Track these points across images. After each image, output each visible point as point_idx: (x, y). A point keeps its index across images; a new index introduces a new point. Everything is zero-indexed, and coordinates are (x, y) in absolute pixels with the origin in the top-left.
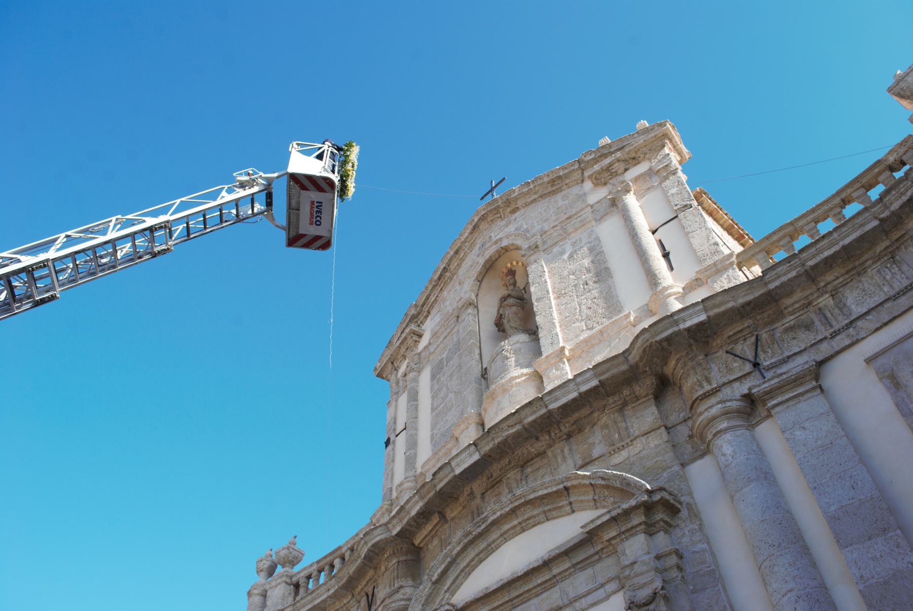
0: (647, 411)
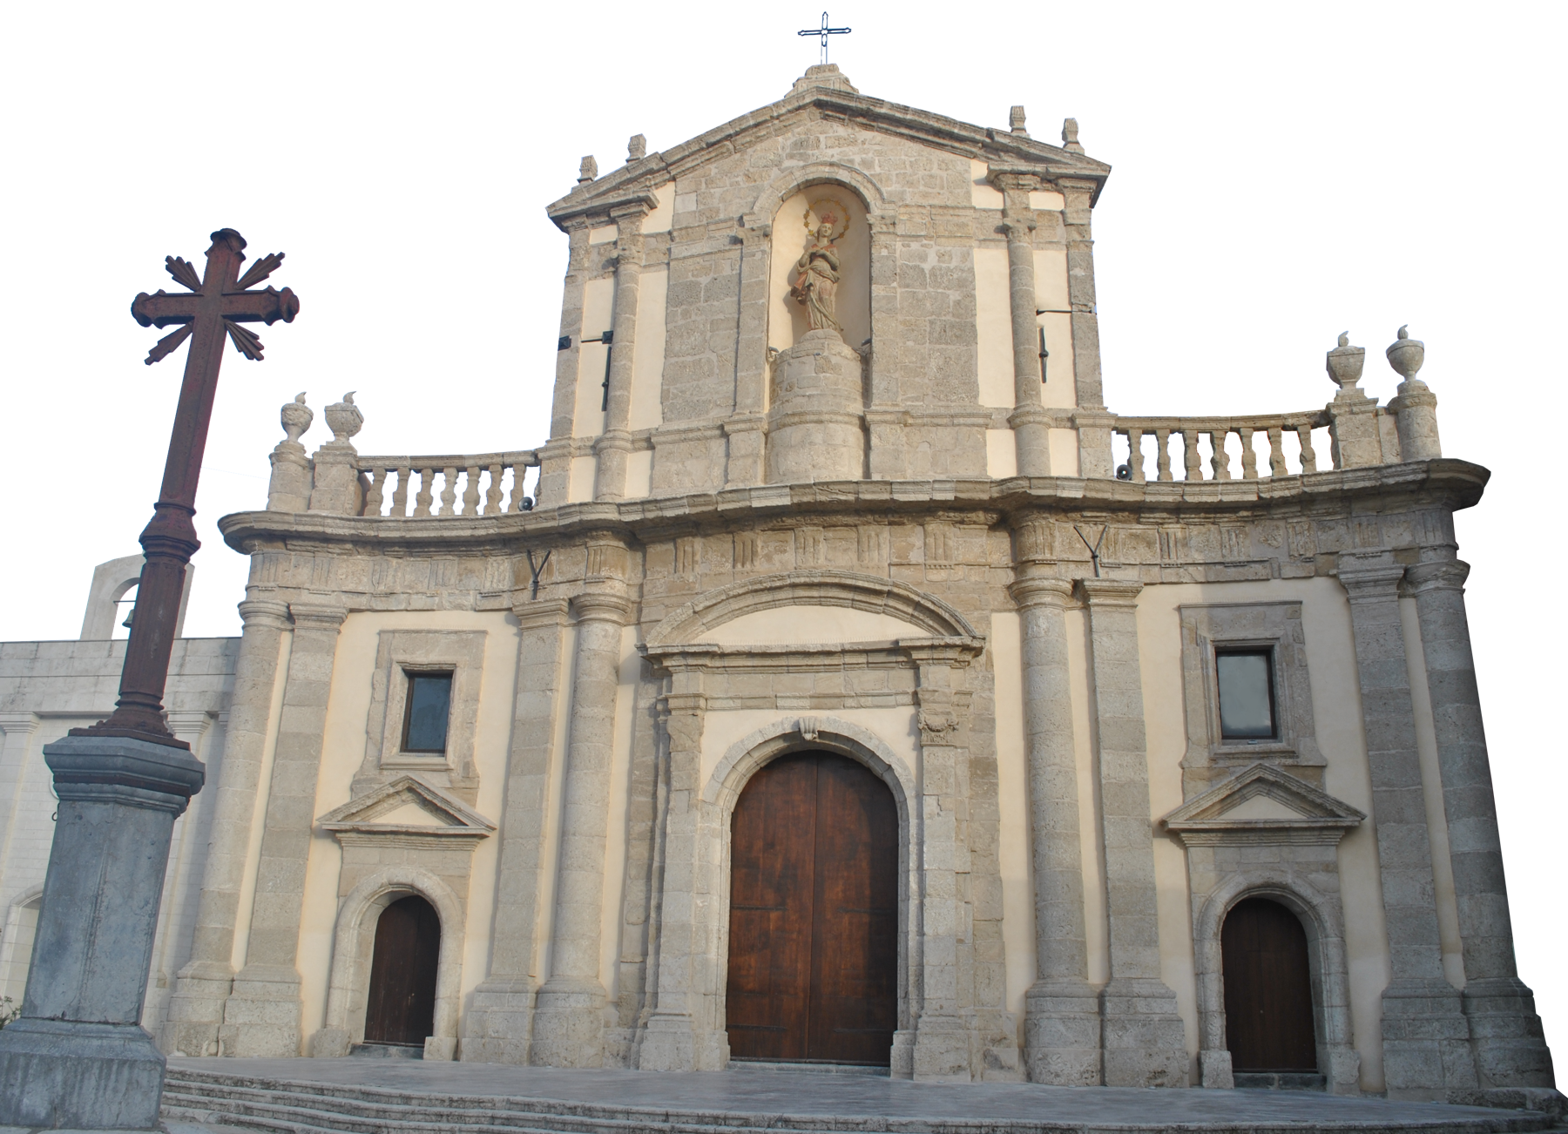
0: (977, 540)
